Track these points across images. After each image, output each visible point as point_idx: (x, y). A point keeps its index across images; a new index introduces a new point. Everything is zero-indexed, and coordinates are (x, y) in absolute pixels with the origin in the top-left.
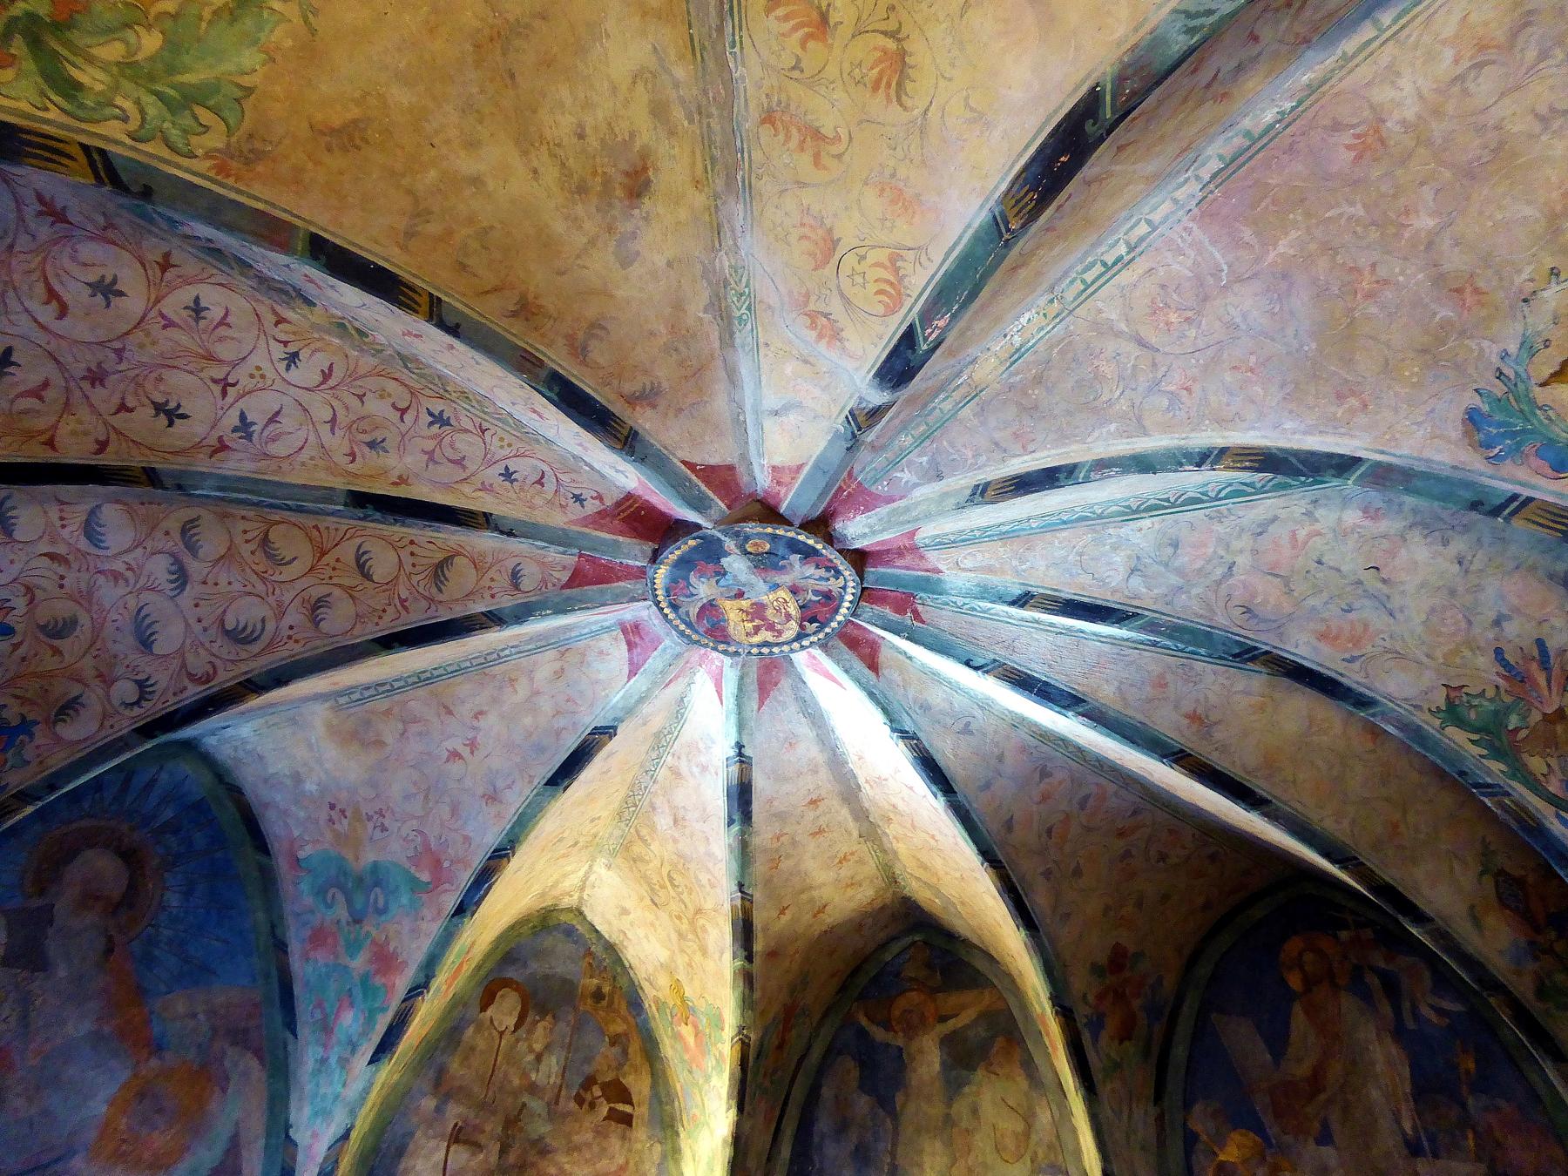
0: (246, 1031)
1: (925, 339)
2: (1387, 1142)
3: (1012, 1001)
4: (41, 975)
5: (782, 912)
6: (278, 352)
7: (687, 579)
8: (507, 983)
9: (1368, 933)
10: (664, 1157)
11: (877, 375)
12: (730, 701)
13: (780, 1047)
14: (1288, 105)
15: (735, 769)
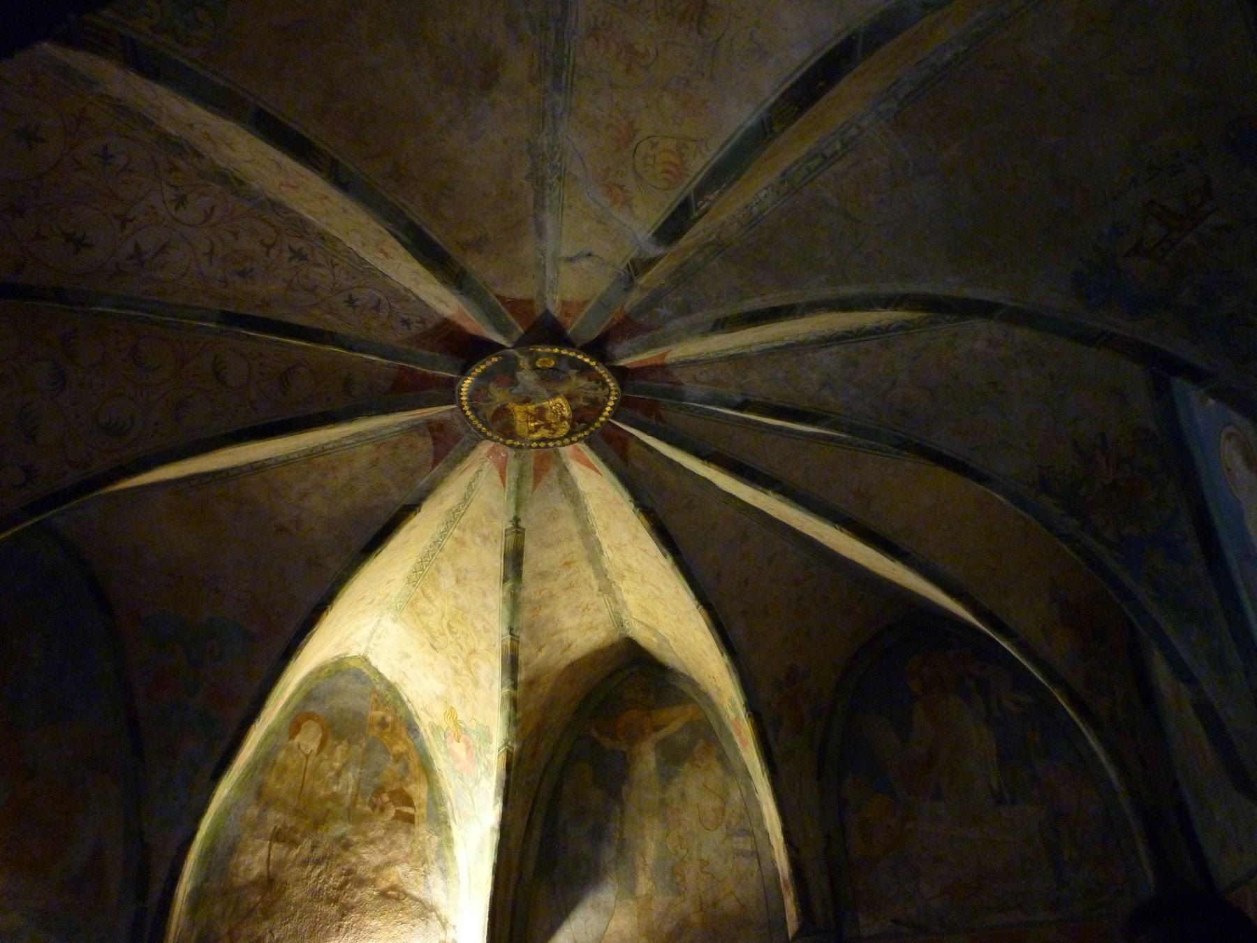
1: (697, 209)
3: (709, 712)
5: (540, 650)
6: (169, 194)
7: (487, 389)
8: (310, 716)
10: (440, 845)
11: (654, 234)
12: (511, 485)
13: (533, 756)
14: (962, 48)
15: (511, 538)
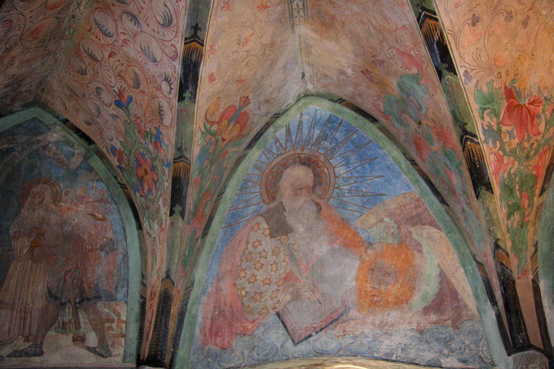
0: (418, 215)
4: (291, 234)
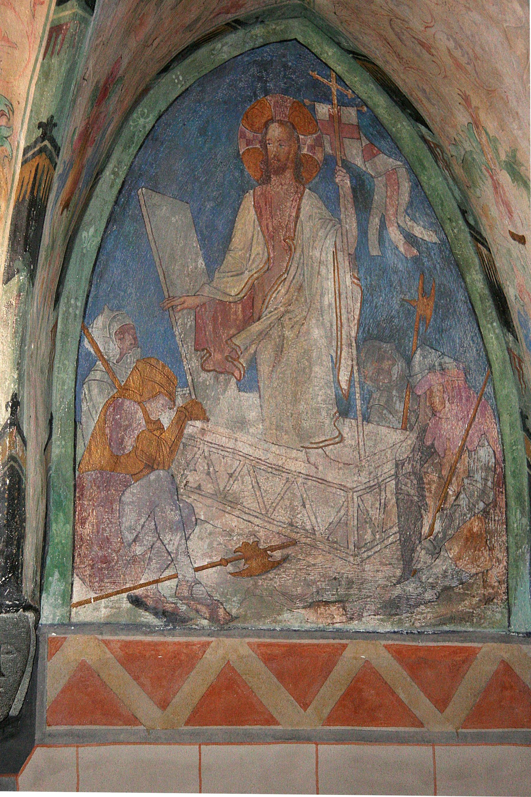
2: (320, 394)
9: (351, 115)
